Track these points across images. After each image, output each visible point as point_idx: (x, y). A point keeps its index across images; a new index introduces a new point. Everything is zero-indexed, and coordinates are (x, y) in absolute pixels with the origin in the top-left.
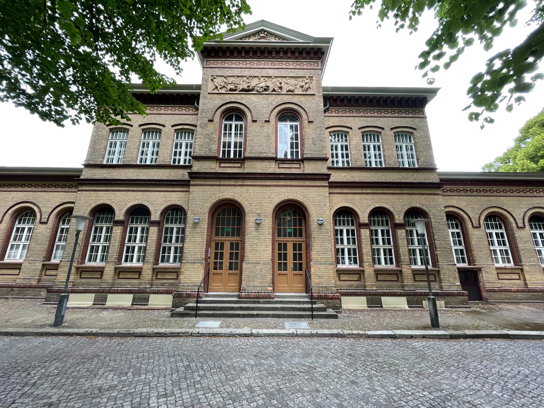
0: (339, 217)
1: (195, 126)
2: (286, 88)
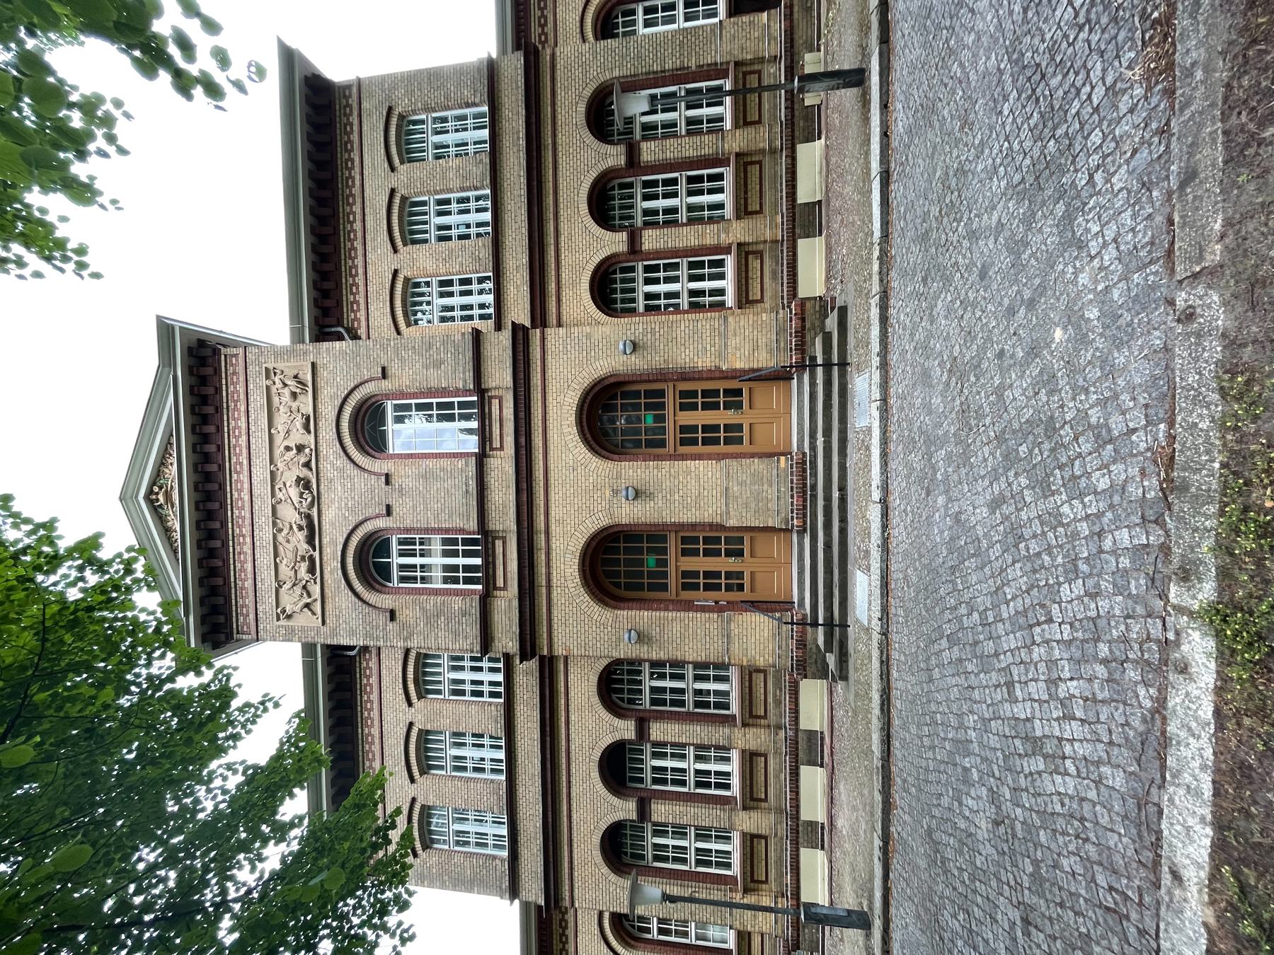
2: (298, 436)
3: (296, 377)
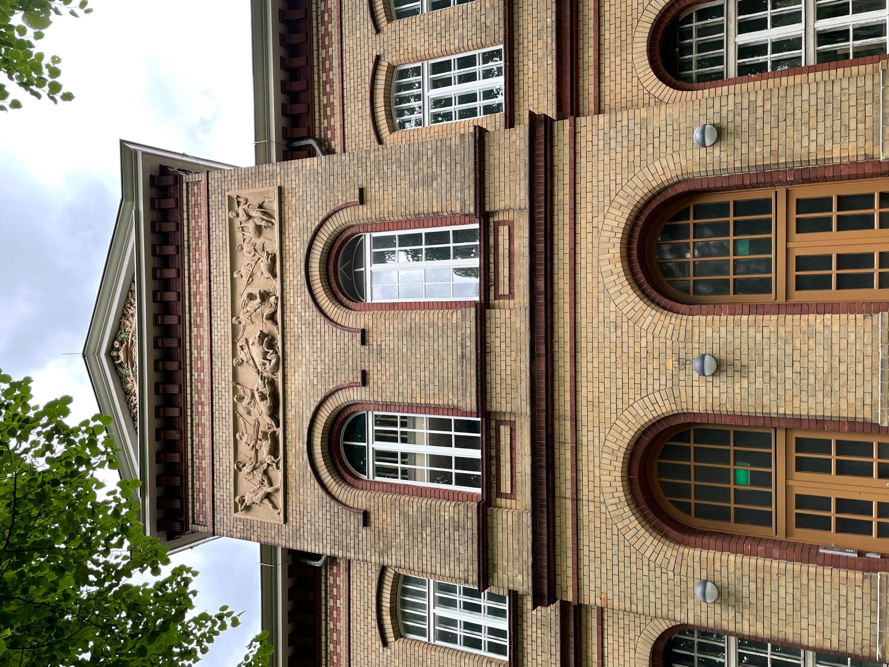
0: (688, 65)
1: (383, 570)
2: (264, 282)
3: (261, 206)
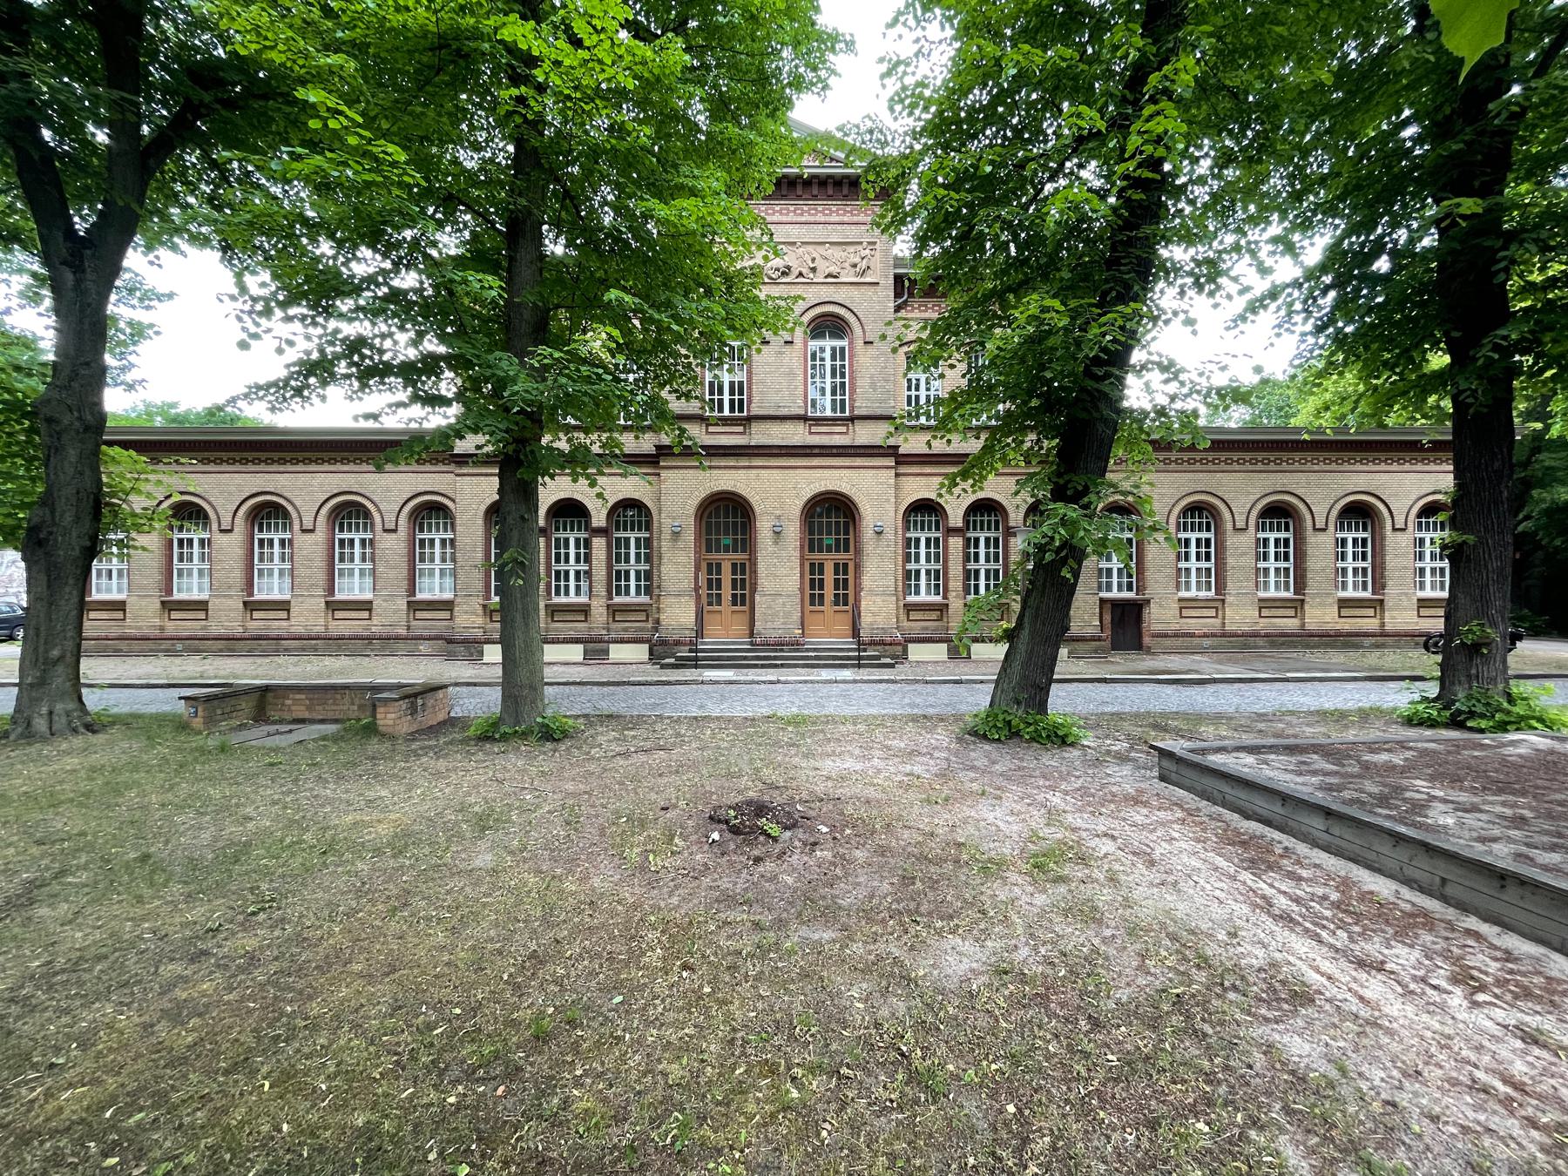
2: (824, 267)
